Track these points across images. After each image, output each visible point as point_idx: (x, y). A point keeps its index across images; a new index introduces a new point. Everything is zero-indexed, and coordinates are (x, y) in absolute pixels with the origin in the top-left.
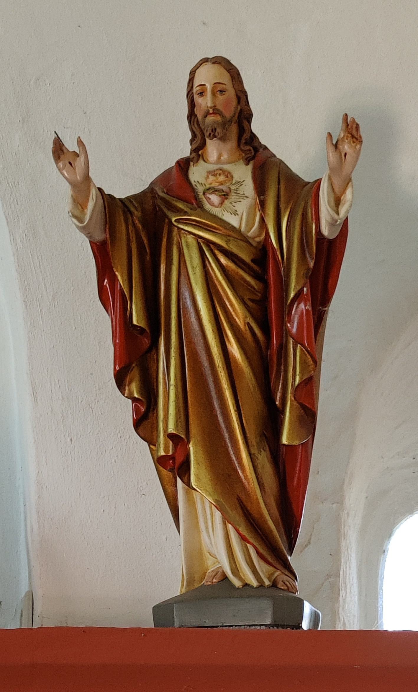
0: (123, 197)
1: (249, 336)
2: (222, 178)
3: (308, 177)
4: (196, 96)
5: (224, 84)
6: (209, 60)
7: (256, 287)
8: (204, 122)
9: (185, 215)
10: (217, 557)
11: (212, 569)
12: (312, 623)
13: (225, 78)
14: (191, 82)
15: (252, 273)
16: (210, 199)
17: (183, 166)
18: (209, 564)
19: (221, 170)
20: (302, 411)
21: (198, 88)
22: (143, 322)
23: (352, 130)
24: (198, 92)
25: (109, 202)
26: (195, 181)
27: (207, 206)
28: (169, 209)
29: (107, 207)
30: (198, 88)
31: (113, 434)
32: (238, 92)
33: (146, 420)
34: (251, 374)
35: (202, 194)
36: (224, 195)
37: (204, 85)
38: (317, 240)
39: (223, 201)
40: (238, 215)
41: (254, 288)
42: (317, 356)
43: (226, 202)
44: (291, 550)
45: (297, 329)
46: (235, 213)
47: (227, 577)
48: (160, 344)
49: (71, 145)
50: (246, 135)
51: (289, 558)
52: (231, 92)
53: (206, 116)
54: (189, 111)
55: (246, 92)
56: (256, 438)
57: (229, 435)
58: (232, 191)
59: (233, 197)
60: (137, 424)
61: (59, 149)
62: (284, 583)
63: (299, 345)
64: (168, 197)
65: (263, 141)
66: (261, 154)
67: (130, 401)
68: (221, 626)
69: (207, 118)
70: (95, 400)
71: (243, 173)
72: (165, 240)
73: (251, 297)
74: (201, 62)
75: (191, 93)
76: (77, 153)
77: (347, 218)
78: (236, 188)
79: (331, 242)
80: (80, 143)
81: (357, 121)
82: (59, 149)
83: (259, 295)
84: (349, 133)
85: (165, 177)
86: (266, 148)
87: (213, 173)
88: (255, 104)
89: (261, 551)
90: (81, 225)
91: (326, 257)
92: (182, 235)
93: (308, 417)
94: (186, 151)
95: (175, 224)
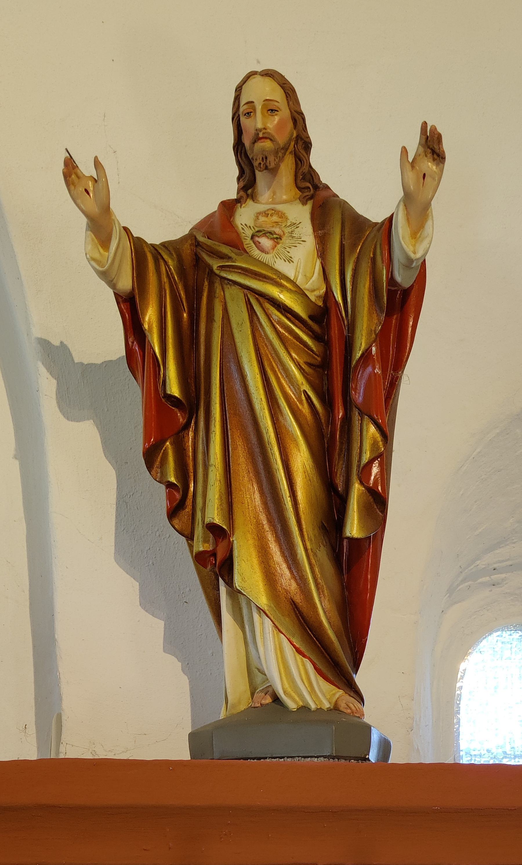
0: (158, 243)
1: (305, 409)
2: (275, 218)
3: (376, 215)
4: (243, 119)
5: (278, 102)
6: (258, 73)
7: (314, 349)
8: (252, 149)
9: (228, 262)
10: (266, 673)
11: (261, 689)
12: (381, 753)
13: (277, 95)
14: (237, 101)
15: (311, 333)
16: (260, 243)
17: (228, 208)
18: (258, 682)
19: (273, 210)
20: (370, 497)
21: (245, 107)
22: (178, 392)
23: (432, 145)
24: (246, 112)
25: (139, 247)
26: (241, 224)
27: (256, 253)
28: (210, 256)
29: (133, 250)
30: (245, 107)
31: (150, 532)
32: (295, 114)
33: (184, 509)
34: (340, 622)
35: (249, 239)
36: (277, 238)
37: (252, 102)
38: (389, 292)
39: (276, 246)
40: (293, 262)
41: (312, 351)
42: (387, 430)
43: (279, 246)
44: (356, 666)
45: (364, 398)
46: (290, 260)
47: (278, 698)
48: (200, 416)
49: (87, 169)
50: (305, 169)
51: (354, 676)
52: (285, 112)
53: (254, 142)
54: (235, 140)
55: (302, 114)
56: (313, 530)
57: (282, 526)
58: (286, 235)
59: (286, 241)
60: (172, 514)
61: (70, 168)
62: (347, 705)
63: (366, 417)
64: (209, 242)
65: (324, 179)
66: (322, 194)
67: (163, 487)
68: (269, 758)
69: (256, 144)
70: (129, 492)
71: (300, 214)
72: (205, 294)
73: (309, 361)
74: (251, 74)
75: (237, 115)
76: (95, 179)
77: (425, 260)
78: (290, 231)
79: (406, 293)
80: (97, 164)
81: (439, 130)
82: (70, 168)
83: (319, 359)
84: (429, 147)
85: (206, 225)
86: (327, 187)
87: (266, 214)
88: (313, 131)
89: (320, 666)
90: (101, 269)
91: (401, 304)
92: (225, 286)
93: (377, 502)
94: (231, 192)
95: (217, 272)
